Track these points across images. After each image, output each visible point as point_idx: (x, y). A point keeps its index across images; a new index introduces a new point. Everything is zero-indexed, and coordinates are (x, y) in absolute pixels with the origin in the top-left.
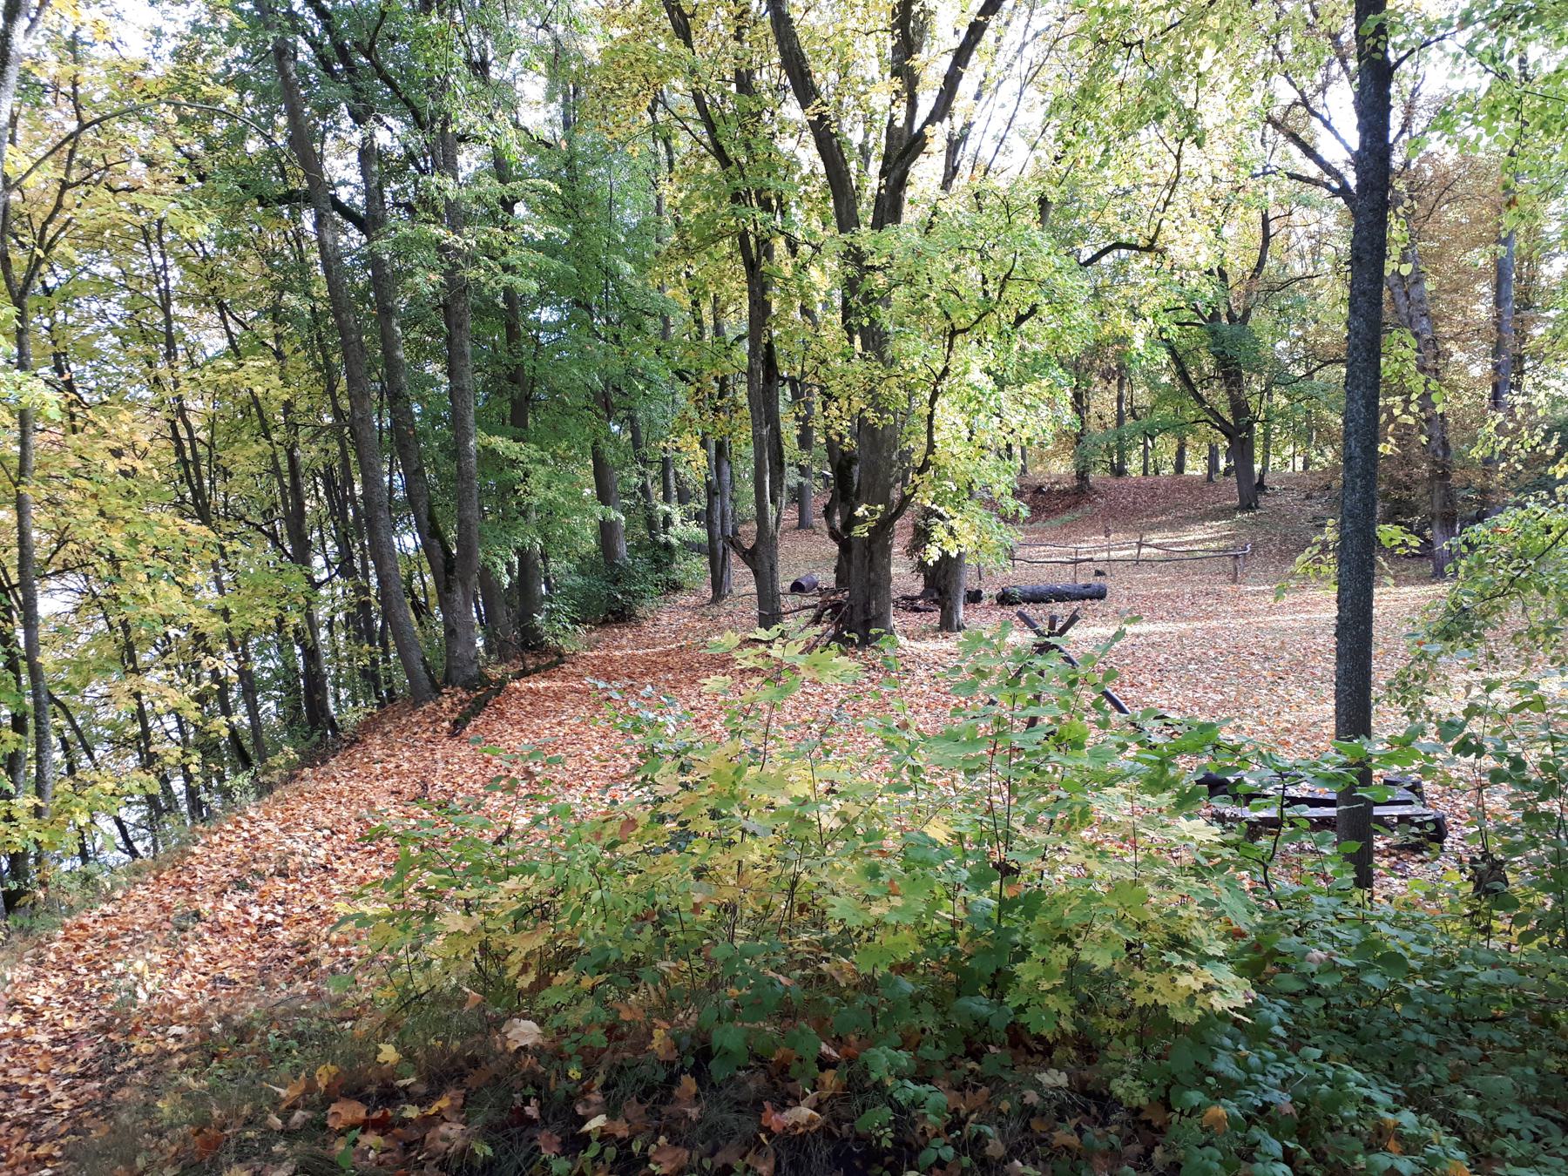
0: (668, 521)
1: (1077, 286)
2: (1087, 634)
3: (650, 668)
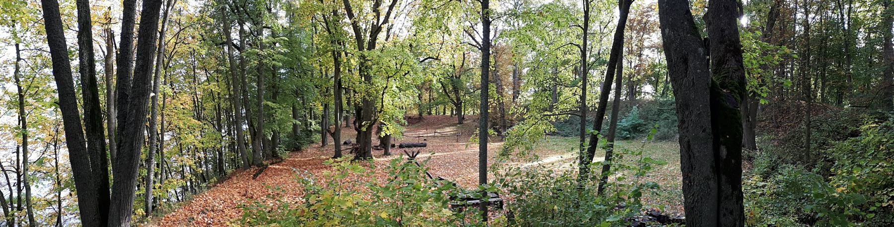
0: (311, 124)
1: (420, 67)
2: (422, 156)
3: (305, 163)
